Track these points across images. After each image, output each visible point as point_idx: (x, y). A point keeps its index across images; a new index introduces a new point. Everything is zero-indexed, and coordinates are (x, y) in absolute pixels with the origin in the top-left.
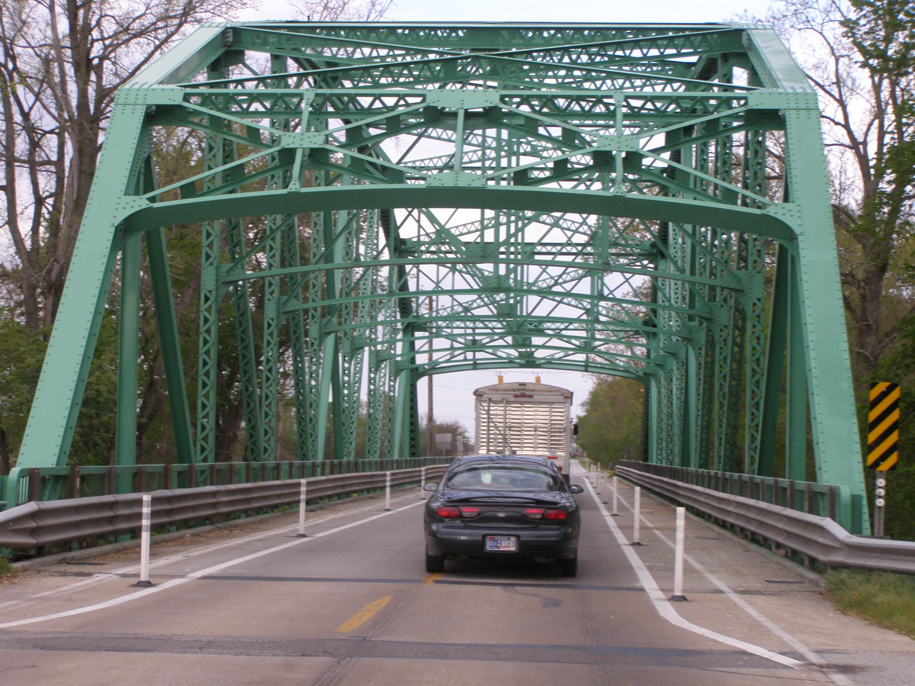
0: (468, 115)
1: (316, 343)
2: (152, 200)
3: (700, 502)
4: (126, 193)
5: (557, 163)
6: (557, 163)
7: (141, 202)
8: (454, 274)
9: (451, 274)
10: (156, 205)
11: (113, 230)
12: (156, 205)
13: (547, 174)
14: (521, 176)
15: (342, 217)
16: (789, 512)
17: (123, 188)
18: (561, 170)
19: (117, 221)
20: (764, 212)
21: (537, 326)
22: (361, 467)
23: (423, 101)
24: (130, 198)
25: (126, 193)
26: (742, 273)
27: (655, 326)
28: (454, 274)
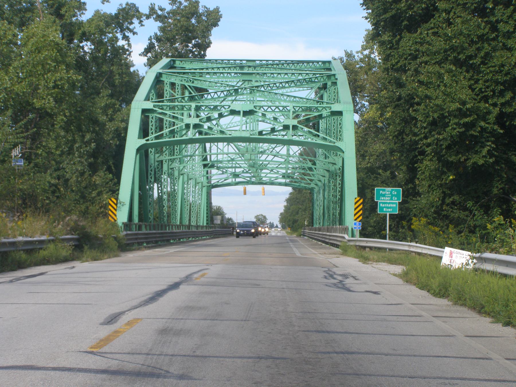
0: (244, 112)
1: (177, 178)
2: (148, 140)
3: (337, 241)
4: (138, 138)
5: (271, 129)
6: (271, 129)
7: (143, 141)
8: (228, 146)
9: (227, 146)
10: (148, 142)
11: (136, 150)
12: (148, 142)
13: (270, 132)
14: (260, 133)
15: (208, 145)
16: (311, 232)
17: (137, 136)
18: (273, 130)
19: (137, 147)
20: (335, 144)
21: (263, 167)
22: (152, 228)
23: (229, 108)
24: (140, 140)
25: (138, 138)
26: (335, 157)
27: (330, 69)
28: (228, 146)
